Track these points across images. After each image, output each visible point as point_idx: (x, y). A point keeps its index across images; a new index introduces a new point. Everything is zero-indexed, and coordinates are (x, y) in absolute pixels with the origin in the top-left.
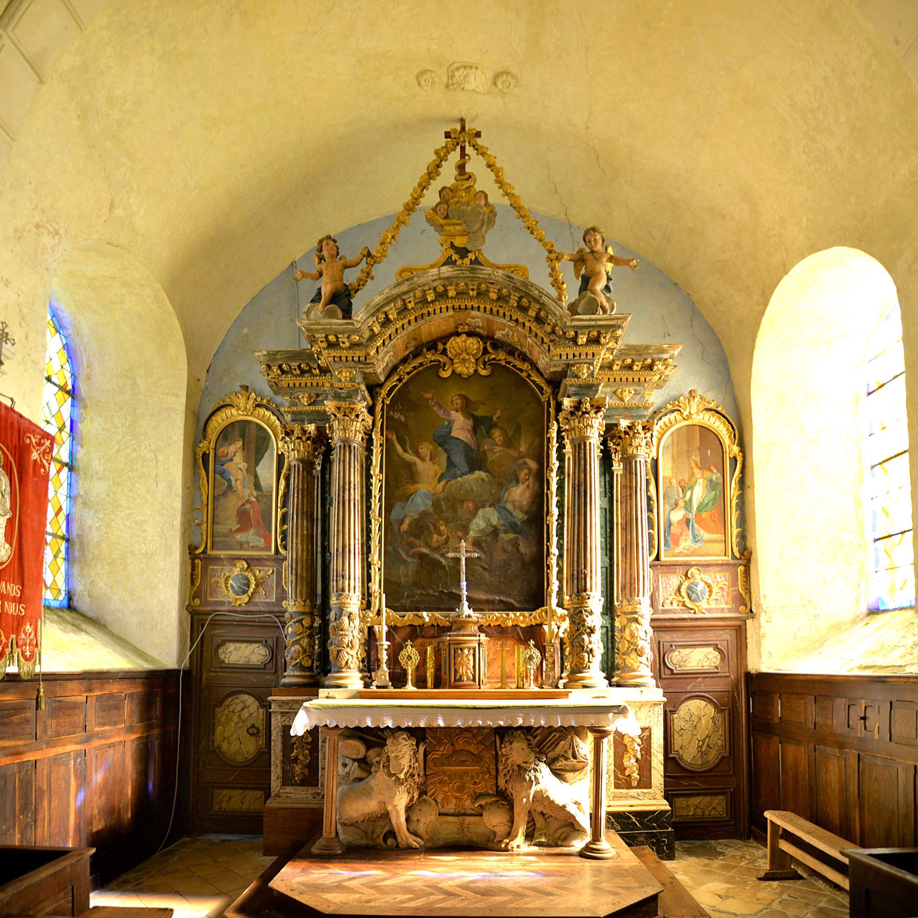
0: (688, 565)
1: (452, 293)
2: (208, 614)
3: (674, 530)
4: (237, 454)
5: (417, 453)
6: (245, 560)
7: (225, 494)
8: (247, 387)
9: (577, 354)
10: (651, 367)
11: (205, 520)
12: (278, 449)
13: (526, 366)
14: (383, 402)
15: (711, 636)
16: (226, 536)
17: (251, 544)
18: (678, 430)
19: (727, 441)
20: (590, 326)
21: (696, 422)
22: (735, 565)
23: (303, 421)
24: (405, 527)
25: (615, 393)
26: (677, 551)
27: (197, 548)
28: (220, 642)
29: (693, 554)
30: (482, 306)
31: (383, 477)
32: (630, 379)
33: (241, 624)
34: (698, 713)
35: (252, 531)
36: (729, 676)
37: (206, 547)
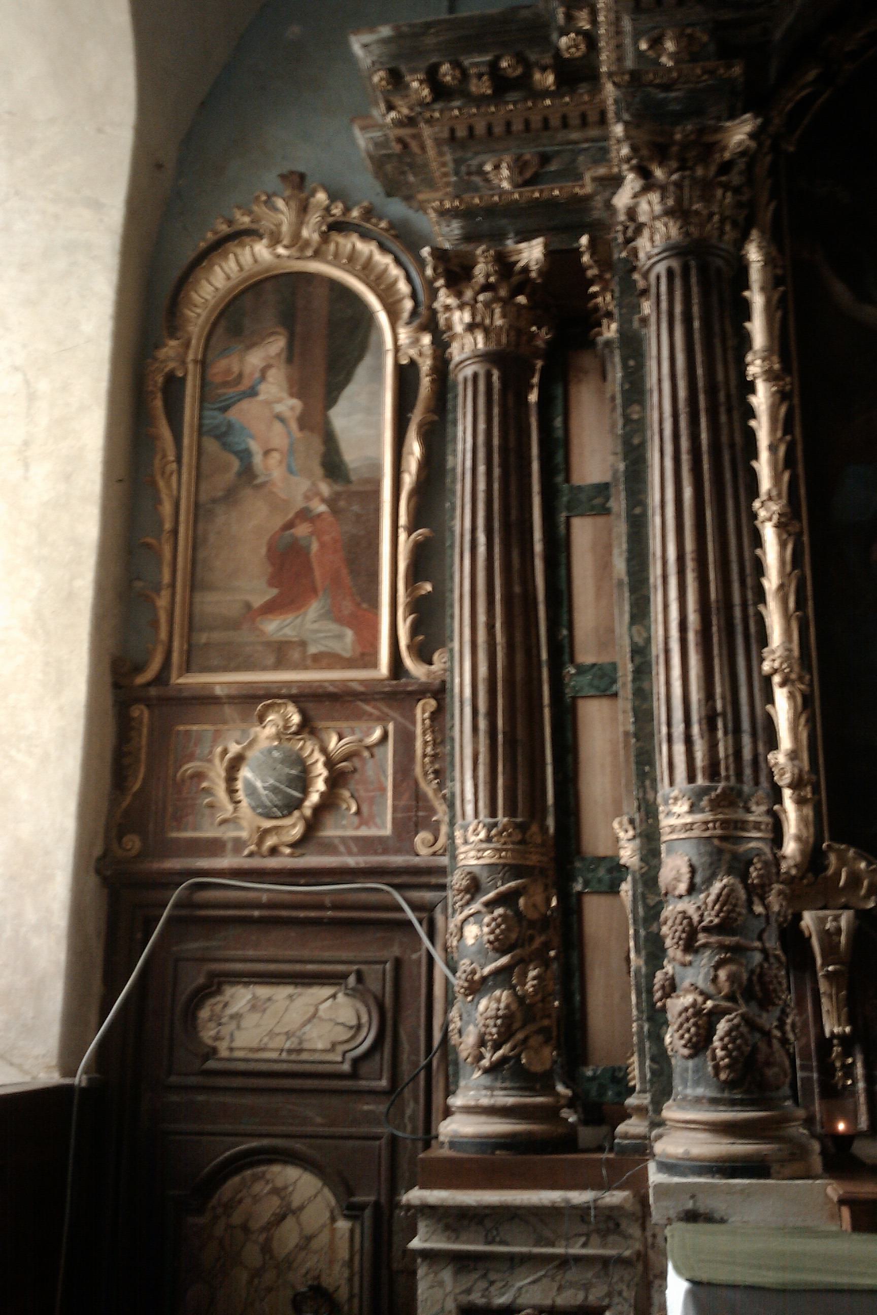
4: (272, 374)
7: (230, 496)
8: (302, 177)
11: (166, 578)
12: (397, 348)
16: (234, 625)
17: (313, 650)
23: (497, 237)
27: (139, 668)
28: (201, 980)
31: (781, 397)
35: (314, 608)
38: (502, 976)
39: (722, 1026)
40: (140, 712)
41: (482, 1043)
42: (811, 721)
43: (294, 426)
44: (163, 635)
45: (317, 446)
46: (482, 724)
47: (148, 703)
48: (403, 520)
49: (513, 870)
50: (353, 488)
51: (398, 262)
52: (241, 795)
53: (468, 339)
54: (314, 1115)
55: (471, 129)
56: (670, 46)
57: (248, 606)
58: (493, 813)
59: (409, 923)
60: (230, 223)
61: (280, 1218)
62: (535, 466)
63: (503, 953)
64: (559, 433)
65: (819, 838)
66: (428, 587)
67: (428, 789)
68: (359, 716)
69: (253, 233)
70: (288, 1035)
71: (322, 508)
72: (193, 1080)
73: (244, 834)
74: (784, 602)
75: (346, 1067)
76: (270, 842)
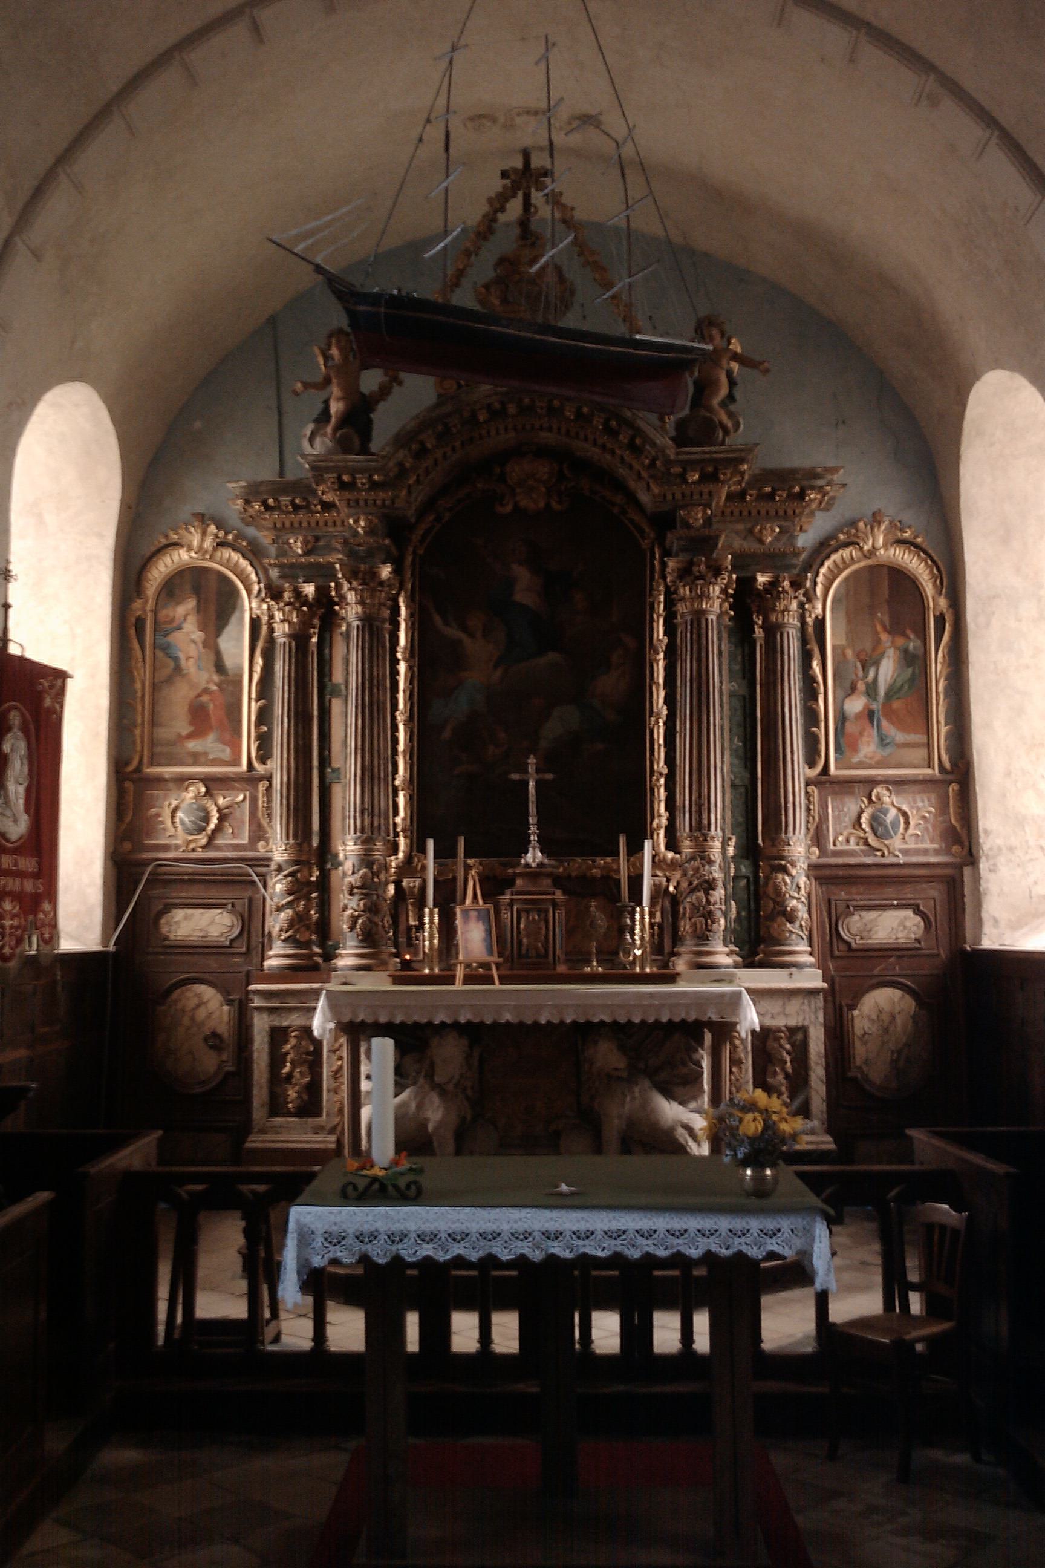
0: (872, 782)
1: (512, 409)
2: (147, 863)
3: (850, 727)
5: (465, 629)
6: (201, 780)
7: (169, 681)
9: (688, 492)
10: (802, 495)
11: (139, 721)
12: (251, 609)
13: (619, 499)
14: (414, 553)
15: (909, 893)
16: (172, 744)
17: (211, 757)
18: (855, 573)
19: (929, 589)
20: (702, 461)
21: (882, 561)
22: (942, 782)
23: (295, 578)
24: (447, 734)
25: (751, 531)
26: (855, 760)
27: (127, 764)
28: (161, 907)
29: (879, 765)
30: (555, 427)
31: (410, 668)
32: (772, 513)
33: (193, 880)
34: (881, 1005)
35: (211, 737)
36: (938, 955)
37: (141, 762)
38: (290, 904)
39: (360, 921)
40: (128, 784)
41: (281, 930)
42: (412, 805)
43: (201, 646)
44: (139, 748)
45: (212, 657)
46: (285, 802)
47: (134, 781)
48: (254, 696)
49: (296, 862)
50: (231, 678)
51: (252, 565)
52: (178, 824)
53: (281, 626)
54: (213, 964)
55: (283, 524)
56: (362, 523)
57: (179, 735)
58: (288, 839)
59: (254, 882)
60: (166, 537)
61: (198, 1006)
62: (316, 673)
63: (290, 895)
64: (327, 657)
65: (411, 850)
66: (265, 728)
67: (264, 822)
68: (233, 788)
69: (177, 545)
70: (201, 930)
71: (215, 688)
72: (160, 950)
73: (179, 842)
74: (404, 757)
75: (227, 943)
76: (192, 846)
